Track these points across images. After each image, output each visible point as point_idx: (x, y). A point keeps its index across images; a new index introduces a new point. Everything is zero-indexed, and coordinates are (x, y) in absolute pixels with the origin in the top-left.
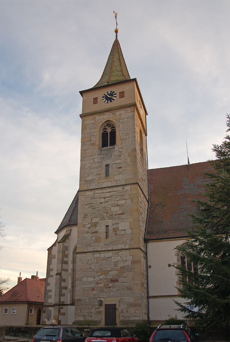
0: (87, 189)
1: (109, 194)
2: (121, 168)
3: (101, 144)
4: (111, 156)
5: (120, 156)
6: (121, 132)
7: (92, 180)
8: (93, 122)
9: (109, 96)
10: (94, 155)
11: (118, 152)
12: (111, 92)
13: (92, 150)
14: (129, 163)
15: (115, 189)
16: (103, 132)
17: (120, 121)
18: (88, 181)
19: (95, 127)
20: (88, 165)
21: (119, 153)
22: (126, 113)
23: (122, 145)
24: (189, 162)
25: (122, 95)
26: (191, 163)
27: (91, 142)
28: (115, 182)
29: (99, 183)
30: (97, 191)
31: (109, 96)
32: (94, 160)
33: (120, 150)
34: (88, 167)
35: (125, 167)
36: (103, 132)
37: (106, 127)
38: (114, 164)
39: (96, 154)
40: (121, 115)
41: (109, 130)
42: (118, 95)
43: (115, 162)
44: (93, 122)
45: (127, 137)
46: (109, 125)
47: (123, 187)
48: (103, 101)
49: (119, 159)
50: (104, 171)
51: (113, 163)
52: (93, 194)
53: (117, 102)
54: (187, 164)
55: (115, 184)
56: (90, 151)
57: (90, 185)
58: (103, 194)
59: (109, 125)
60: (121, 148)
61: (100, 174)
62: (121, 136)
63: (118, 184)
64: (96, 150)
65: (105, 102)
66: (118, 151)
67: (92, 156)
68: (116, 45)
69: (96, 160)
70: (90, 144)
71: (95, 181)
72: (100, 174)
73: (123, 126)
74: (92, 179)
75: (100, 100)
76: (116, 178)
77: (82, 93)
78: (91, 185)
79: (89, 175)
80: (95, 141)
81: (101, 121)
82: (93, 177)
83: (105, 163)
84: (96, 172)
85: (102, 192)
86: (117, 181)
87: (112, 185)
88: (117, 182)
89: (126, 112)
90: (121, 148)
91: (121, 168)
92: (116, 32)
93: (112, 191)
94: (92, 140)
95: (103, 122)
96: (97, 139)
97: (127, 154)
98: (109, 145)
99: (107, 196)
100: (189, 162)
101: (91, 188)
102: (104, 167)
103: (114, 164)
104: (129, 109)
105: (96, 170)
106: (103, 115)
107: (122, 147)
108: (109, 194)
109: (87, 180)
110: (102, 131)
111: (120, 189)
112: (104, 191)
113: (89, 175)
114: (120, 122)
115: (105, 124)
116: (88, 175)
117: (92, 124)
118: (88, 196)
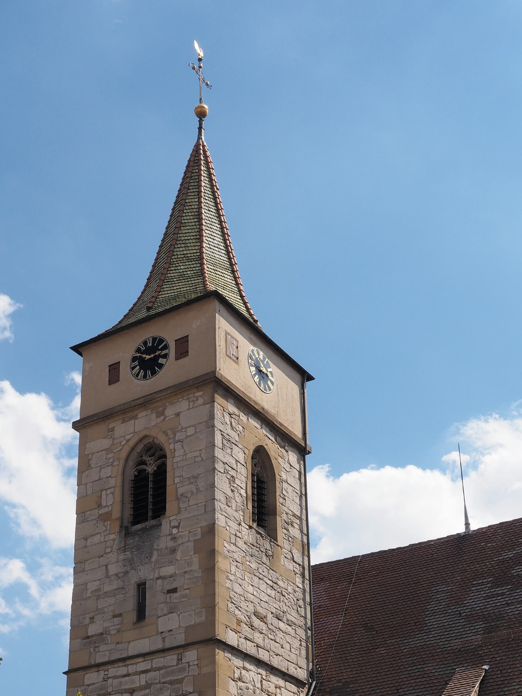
0: (86, 664)
1: (143, 679)
2: (174, 591)
3: (129, 512)
4: (151, 554)
5: (173, 551)
6: (177, 474)
7: (102, 634)
8: (106, 443)
9: (148, 357)
10: (107, 553)
11: (169, 538)
12: (154, 339)
13: (103, 537)
14: (196, 574)
15: (158, 661)
16: (136, 473)
17: (175, 435)
18: (92, 636)
19: (111, 460)
20: (92, 586)
21: (171, 544)
22: (193, 408)
23: (179, 517)
24: (467, 524)
25: (183, 346)
26: (474, 527)
27: (101, 512)
28: (159, 638)
29: (118, 643)
30: (113, 671)
31: (148, 357)
32: (107, 569)
33: (175, 531)
34: (92, 592)
35: (186, 587)
36: (136, 473)
37: (144, 458)
38: (157, 579)
39: (112, 547)
40: (178, 414)
41: (150, 469)
42: (172, 351)
43: (162, 574)
44: (106, 443)
45: (193, 487)
46: (151, 452)
47: (178, 654)
48: (134, 371)
49: (171, 563)
50: (131, 605)
51: (156, 576)
52: (105, 680)
53: (172, 371)
54: (461, 529)
55: (160, 646)
56: (97, 539)
57: (97, 649)
58: (127, 678)
59: (151, 452)
60: (177, 527)
61: (120, 615)
62: (178, 486)
63: (168, 645)
64: (114, 537)
65: (137, 376)
66: (169, 535)
67: (102, 556)
68: (197, 159)
69: (113, 569)
70: (100, 515)
71: (109, 637)
72: (120, 615)
73: (182, 453)
74: (102, 631)
75: (125, 370)
76: (163, 624)
77: (77, 349)
78: (99, 651)
79: (93, 618)
80: (110, 507)
81: (128, 441)
82: (105, 626)
83: (134, 578)
84: (111, 608)
85: (125, 672)
86: (164, 635)
87: (153, 648)
88: (164, 638)
89: (191, 404)
90: (176, 524)
91: (174, 591)
92: (201, 115)
93: (149, 668)
94: (104, 503)
95: (131, 444)
96: (115, 500)
97: (191, 545)
98: (150, 514)
99: (138, 685)
100: (467, 524)
101: (99, 660)
102: (132, 592)
103: (157, 579)
104: (200, 393)
105: (112, 600)
106: (133, 420)
107: (179, 523)
108: (143, 679)
109: (90, 634)
110: (131, 473)
111: (171, 659)
112: (131, 669)
113: (93, 618)
114: (177, 438)
115: (140, 447)
116: (90, 618)
117: (104, 452)
118: (90, 687)
